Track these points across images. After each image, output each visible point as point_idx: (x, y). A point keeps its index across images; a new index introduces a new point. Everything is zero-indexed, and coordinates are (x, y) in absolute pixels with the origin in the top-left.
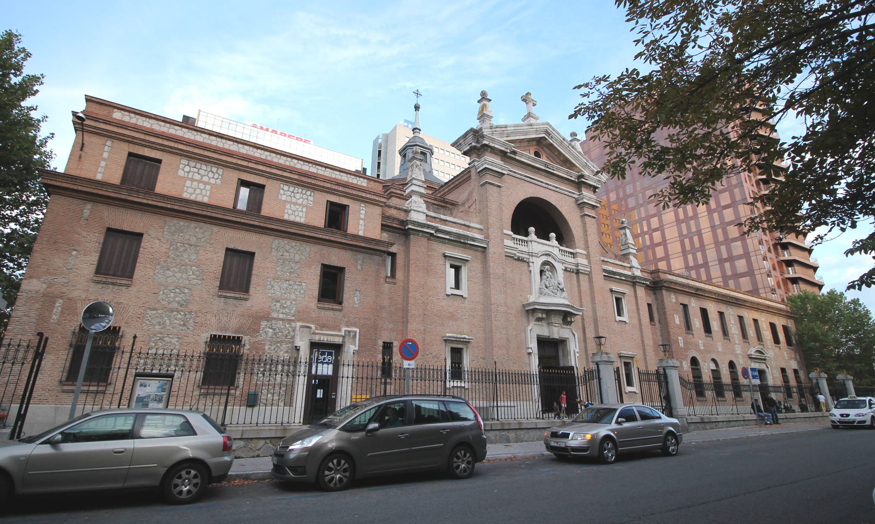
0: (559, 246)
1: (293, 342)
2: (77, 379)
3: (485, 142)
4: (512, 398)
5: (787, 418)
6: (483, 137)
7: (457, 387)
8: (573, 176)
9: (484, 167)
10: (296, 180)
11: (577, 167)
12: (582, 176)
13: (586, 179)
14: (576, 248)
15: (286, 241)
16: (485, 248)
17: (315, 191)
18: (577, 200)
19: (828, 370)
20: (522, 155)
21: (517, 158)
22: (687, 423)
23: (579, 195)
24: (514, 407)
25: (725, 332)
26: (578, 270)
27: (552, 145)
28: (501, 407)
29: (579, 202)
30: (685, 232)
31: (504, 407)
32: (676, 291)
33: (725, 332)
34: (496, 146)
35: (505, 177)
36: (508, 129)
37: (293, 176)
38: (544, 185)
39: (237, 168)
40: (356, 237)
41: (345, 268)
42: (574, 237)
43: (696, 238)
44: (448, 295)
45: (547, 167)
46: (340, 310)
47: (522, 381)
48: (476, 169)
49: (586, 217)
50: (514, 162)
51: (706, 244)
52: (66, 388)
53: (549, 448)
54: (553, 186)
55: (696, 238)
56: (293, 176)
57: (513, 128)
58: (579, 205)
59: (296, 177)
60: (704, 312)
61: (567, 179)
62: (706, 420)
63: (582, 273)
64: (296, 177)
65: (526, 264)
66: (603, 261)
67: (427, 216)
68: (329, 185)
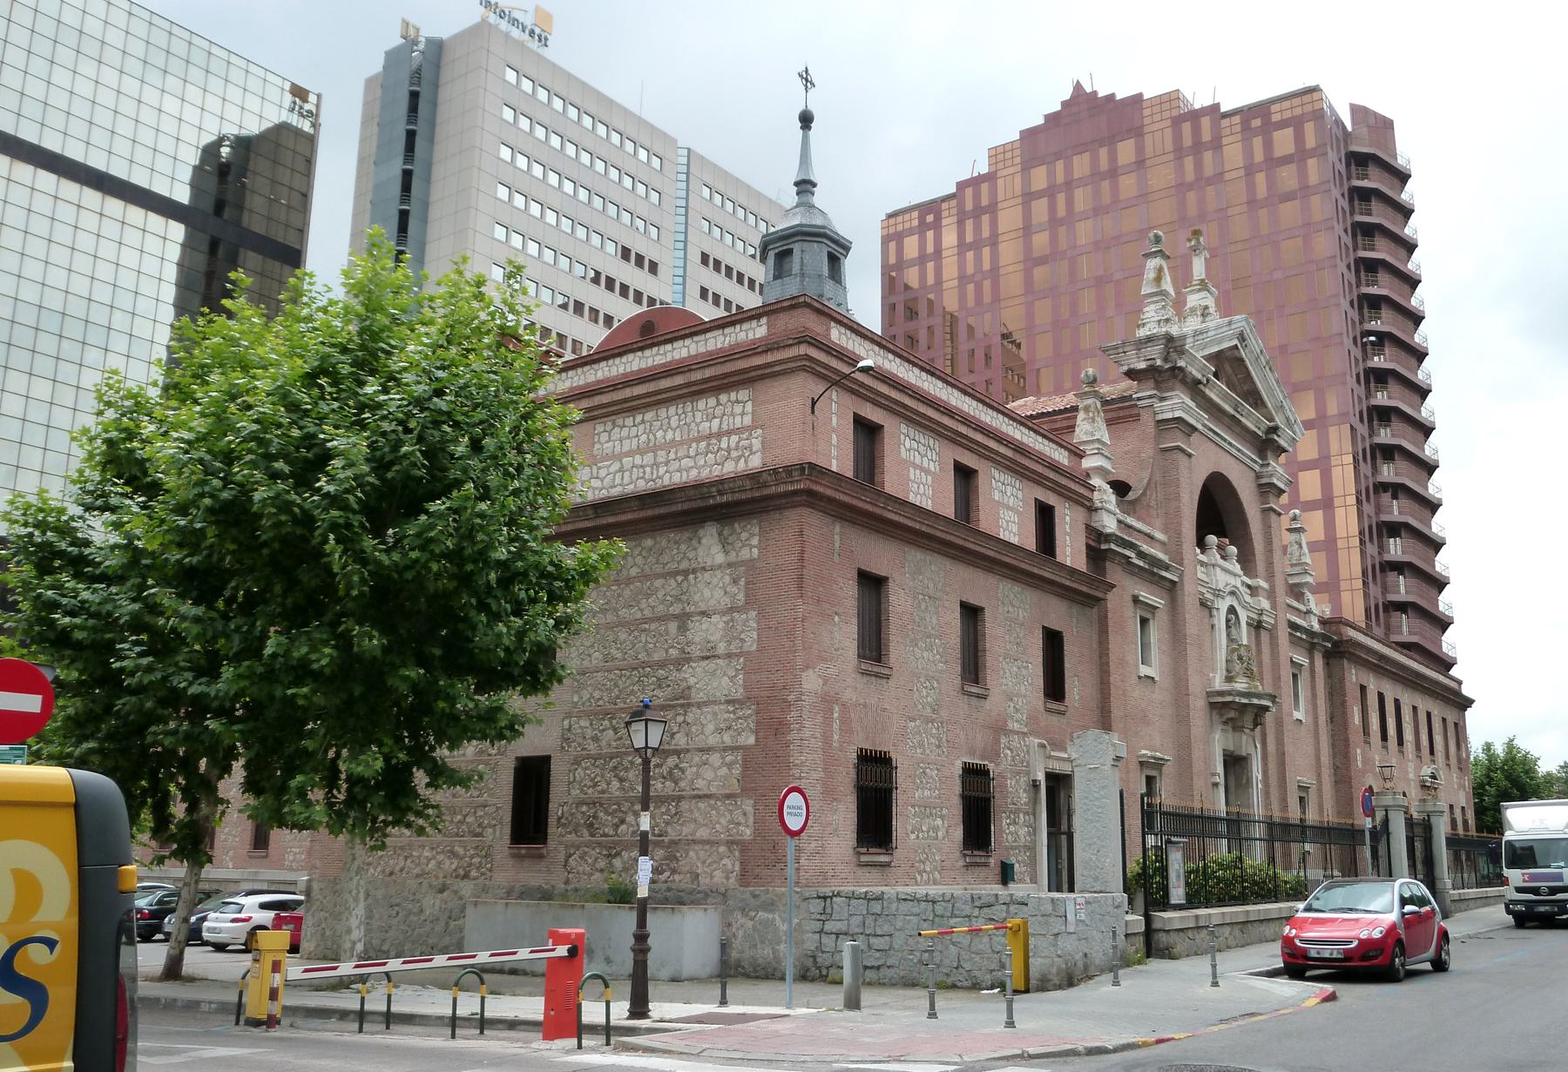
0: (1241, 573)
1: (1028, 773)
2: (546, 834)
3: (1181, 363)
6: (1181, 352)
8: (1252, 420)
9: (1177, 414)
10: (1010, 459)
11: (1266, 407)
12: (1275, 429)
14: (1257, 576)
15: (1017, 588)
16: (1174, 583)
17: (1025, 481)
18: (1258, 476)
19: (26, 510)
23: (1262, 466)
25: (1401, 742)
26: (1260, 622)
27: (1242, 360)
29: (1264, 481)
30: (970, 270)
32: (1366, 665)
33: (1401, 742)
35: (1195, 436)
36: (1210, 334)
37: (1002, 450)
39: (955, 439)
40: (1063, 566)
41: (887, 578)
42: (1254, 555)
43: (987, 284)
44: (1140, 677)
46: (1062, 713)
48: (1155, 413)
49: (1272, 514)
51: (944, 278)
52: (864, 859)
53: (1509, 911)
55: (987, 284)
56: (1002, 450)
58: (1260, 486)
59: (1009, 453)
60: (1381, 697)
63: (1265, 628)
64: (1009, 453)
65: (1207, 611)
66: (1289, 606)
67: (1119, 522)
68: (1039, 469)
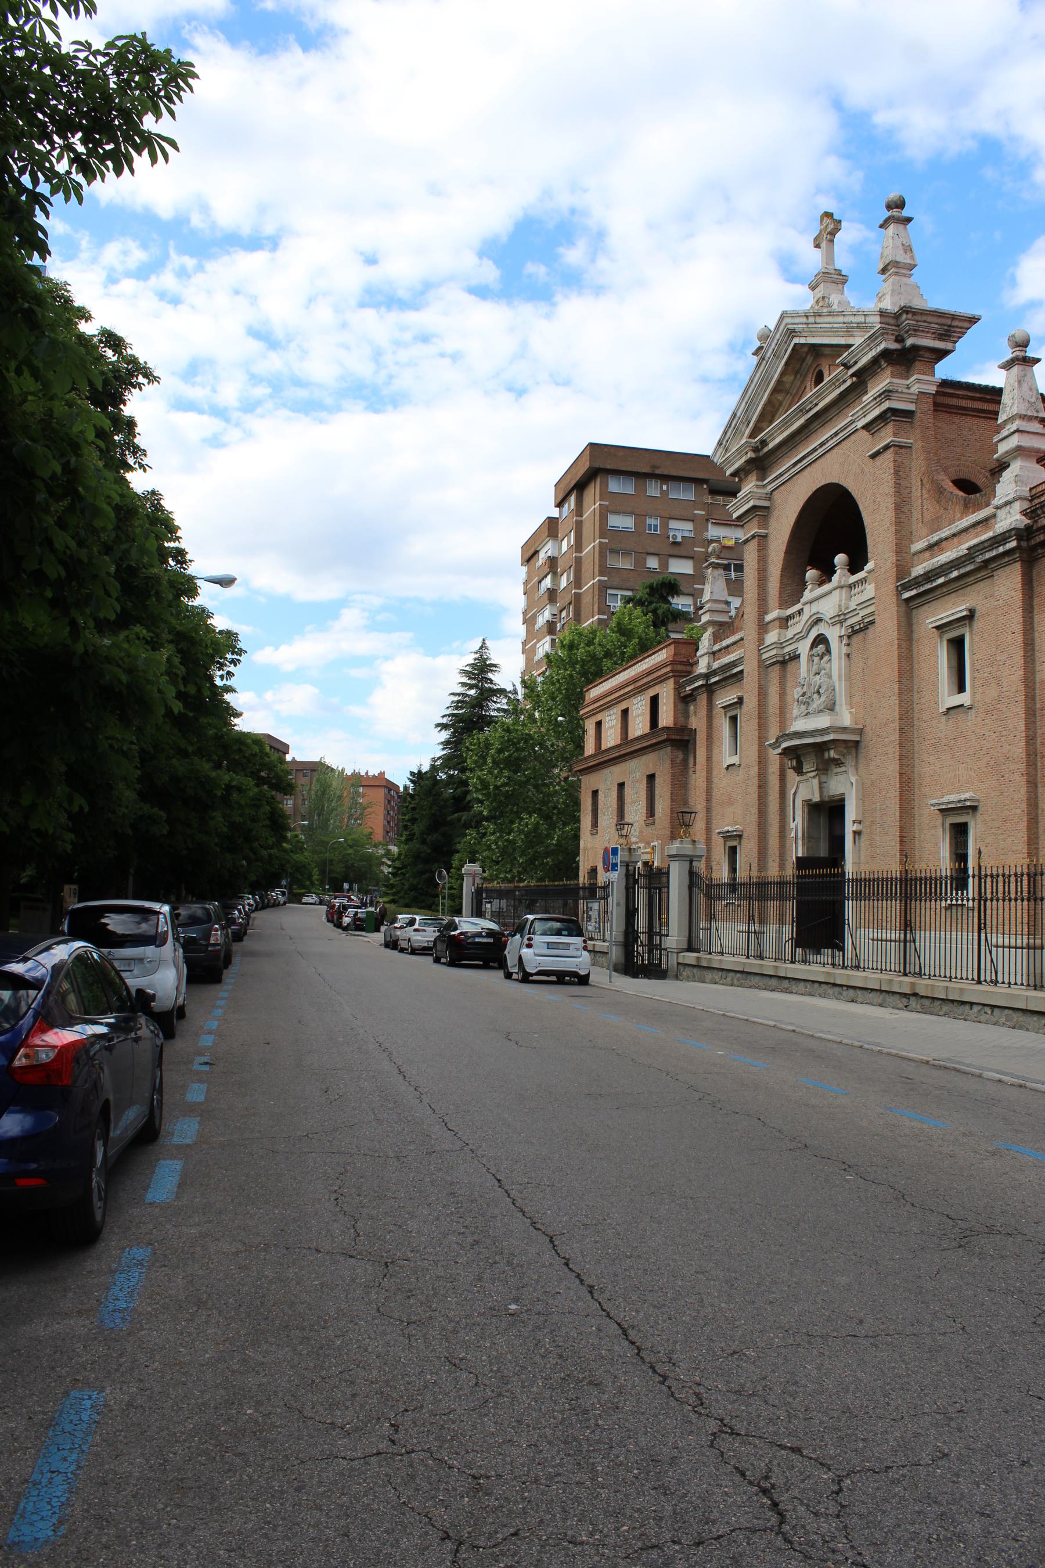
4: (871, 925)
5: (915, 995)
7: (957, 905)
9: (751, 504)
10: (635, 689)
13: (856, 363)
20: (772, 436)
21: (771, 446)
22: (678, 964)
24: (900, 942)
28: (1003, 947)
31: (1010, 947)
34: (736, 466)
38: (820, 451)
45: (808, 412)
47: (911, 894)
50: (779, 454)
54: (832, 437)
57: (744, 404)
61: (842, 396)
62: (704, 964)
